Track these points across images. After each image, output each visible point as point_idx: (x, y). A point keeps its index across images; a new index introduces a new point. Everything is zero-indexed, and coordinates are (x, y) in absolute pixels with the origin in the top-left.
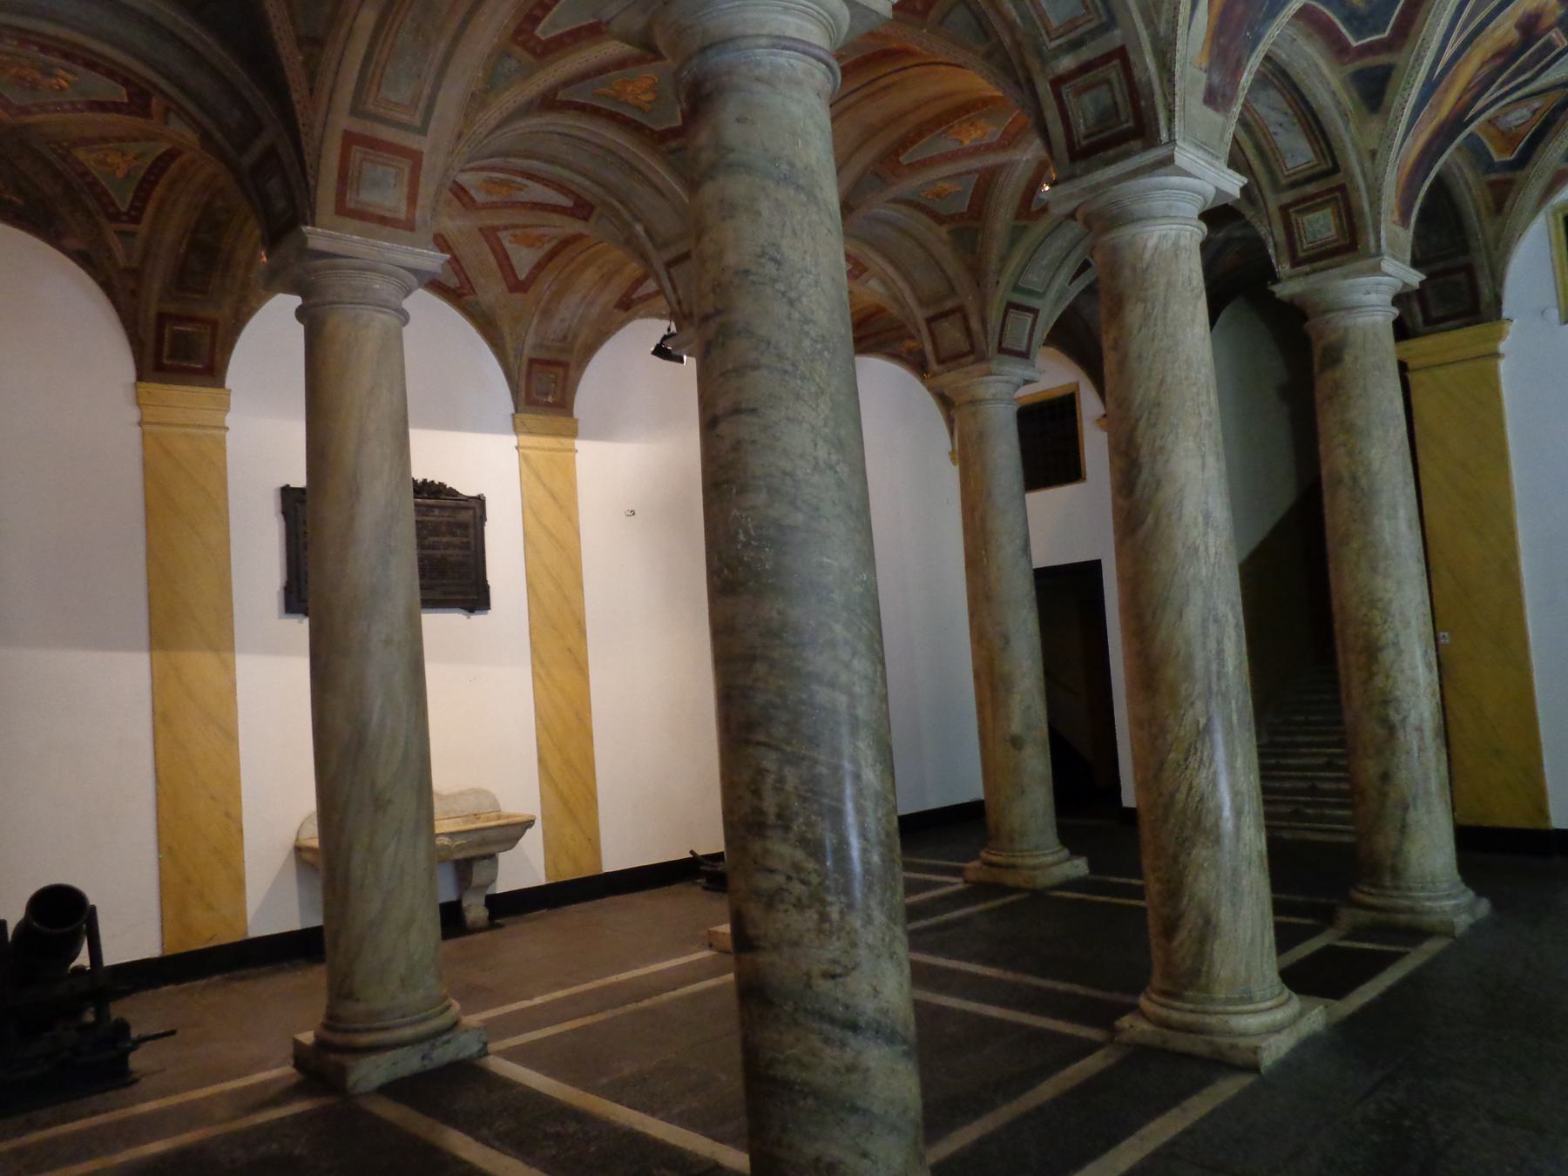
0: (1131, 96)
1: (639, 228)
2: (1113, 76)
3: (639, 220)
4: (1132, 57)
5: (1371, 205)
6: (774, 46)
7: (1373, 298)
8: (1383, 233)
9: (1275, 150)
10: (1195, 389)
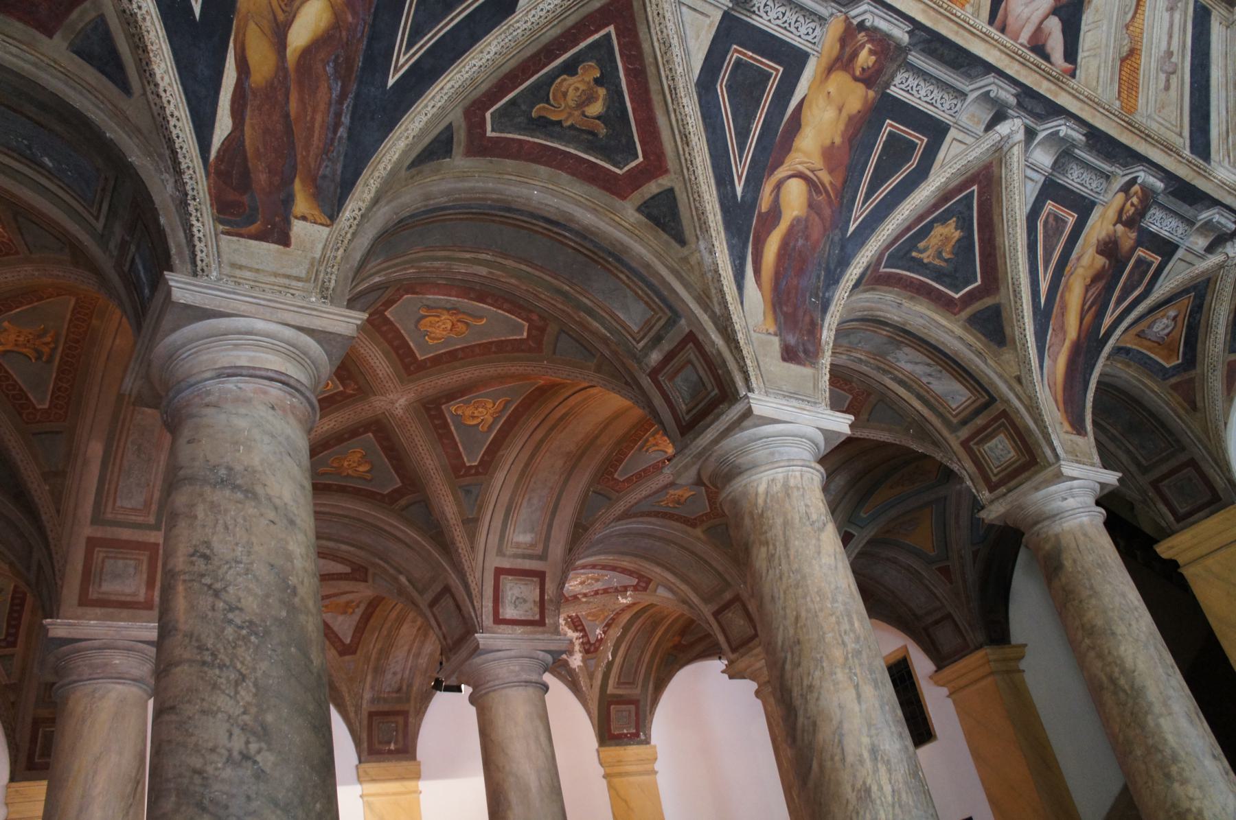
0: (710, 369)
1: (403, 579)
2: (692, 357)
3: (401, 573)
4: (700, 337)
5: (1036, 422)
6: (219, 376)
7: (1071, 502)
8: (1056, 443)
9: (937, 397)
10: (833, 619)
